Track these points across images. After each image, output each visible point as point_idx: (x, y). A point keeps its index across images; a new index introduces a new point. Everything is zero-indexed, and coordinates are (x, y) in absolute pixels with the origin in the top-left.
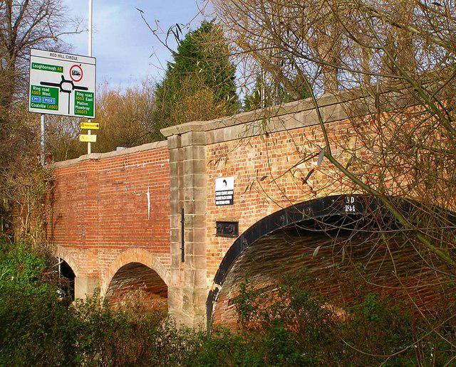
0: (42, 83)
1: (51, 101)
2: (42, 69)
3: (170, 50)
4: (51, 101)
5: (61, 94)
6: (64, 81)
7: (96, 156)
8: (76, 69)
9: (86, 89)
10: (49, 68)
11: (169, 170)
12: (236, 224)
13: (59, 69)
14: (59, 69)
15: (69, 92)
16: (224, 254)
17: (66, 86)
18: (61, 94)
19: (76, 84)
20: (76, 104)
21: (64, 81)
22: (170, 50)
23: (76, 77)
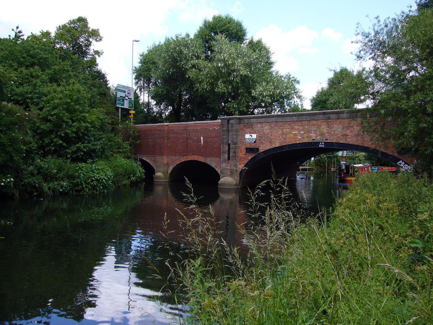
0: (120, 96)
1: (122, 103)
2: (120, 91)
3: (140, 295)
4: (122, 103)
5: (125, 100)
6: (126, 96)
7: (309, 172)
8: (129, 92)
9: (131, 99)
10: (121, 91)
11: (397, 185)
12: (258, 149)
13: (125, 92)
14: (125, 92)
15: (127, 100)
16: (365, 145)
17: (127, 98)
18: (125, 100)
19: (129, 97)
20: (129, 104)
21: (126, 96)
22: (140, 295)
23: (129, 95)
